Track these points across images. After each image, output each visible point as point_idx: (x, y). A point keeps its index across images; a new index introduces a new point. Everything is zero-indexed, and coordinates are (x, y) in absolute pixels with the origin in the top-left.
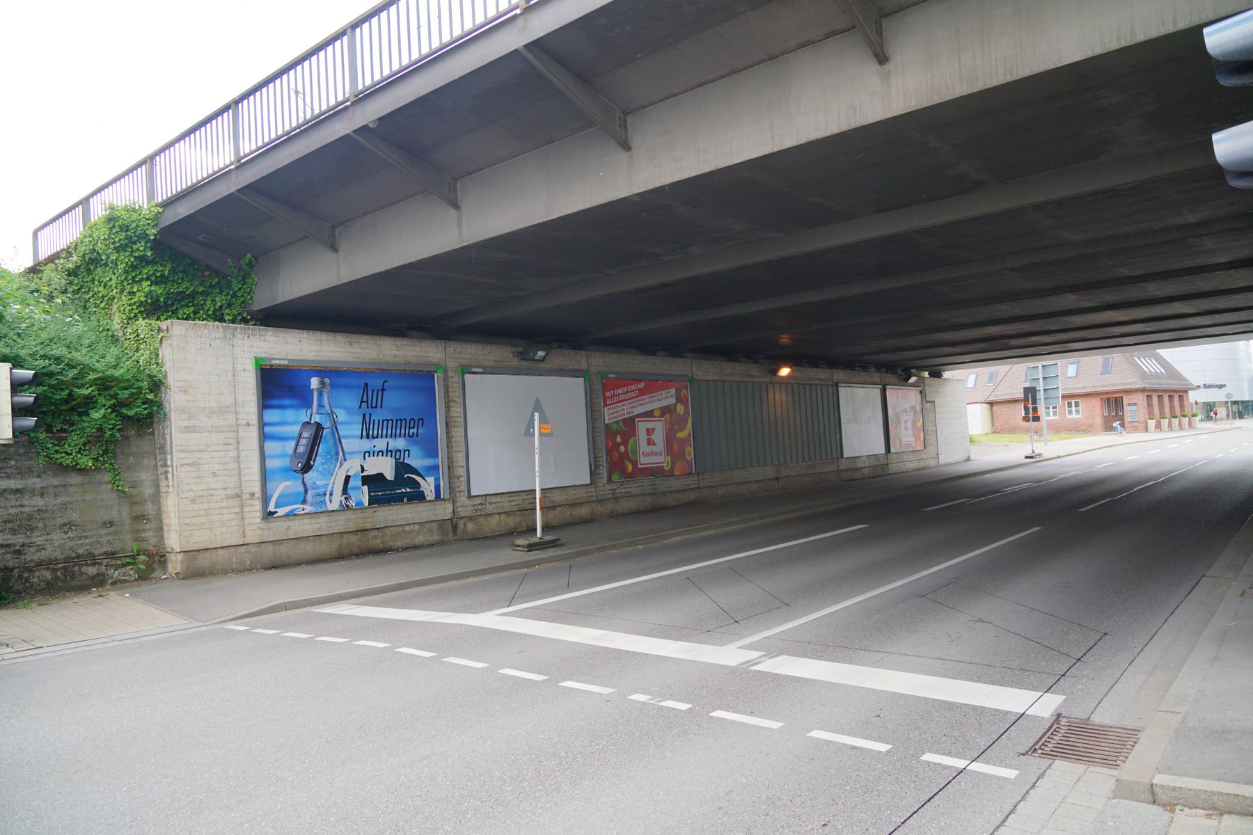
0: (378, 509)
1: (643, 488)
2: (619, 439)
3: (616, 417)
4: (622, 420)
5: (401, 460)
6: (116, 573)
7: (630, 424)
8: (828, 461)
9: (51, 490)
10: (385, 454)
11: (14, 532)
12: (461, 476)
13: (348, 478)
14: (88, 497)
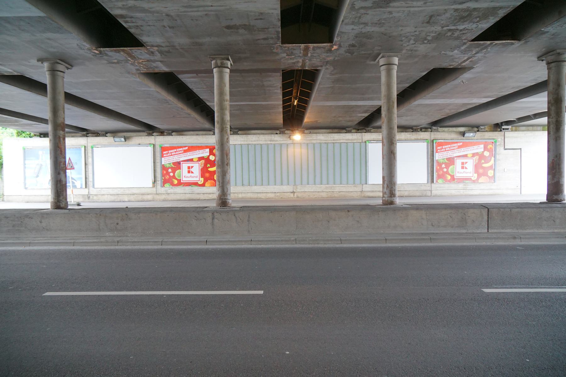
2: (170, 170)
7: (177, 165)
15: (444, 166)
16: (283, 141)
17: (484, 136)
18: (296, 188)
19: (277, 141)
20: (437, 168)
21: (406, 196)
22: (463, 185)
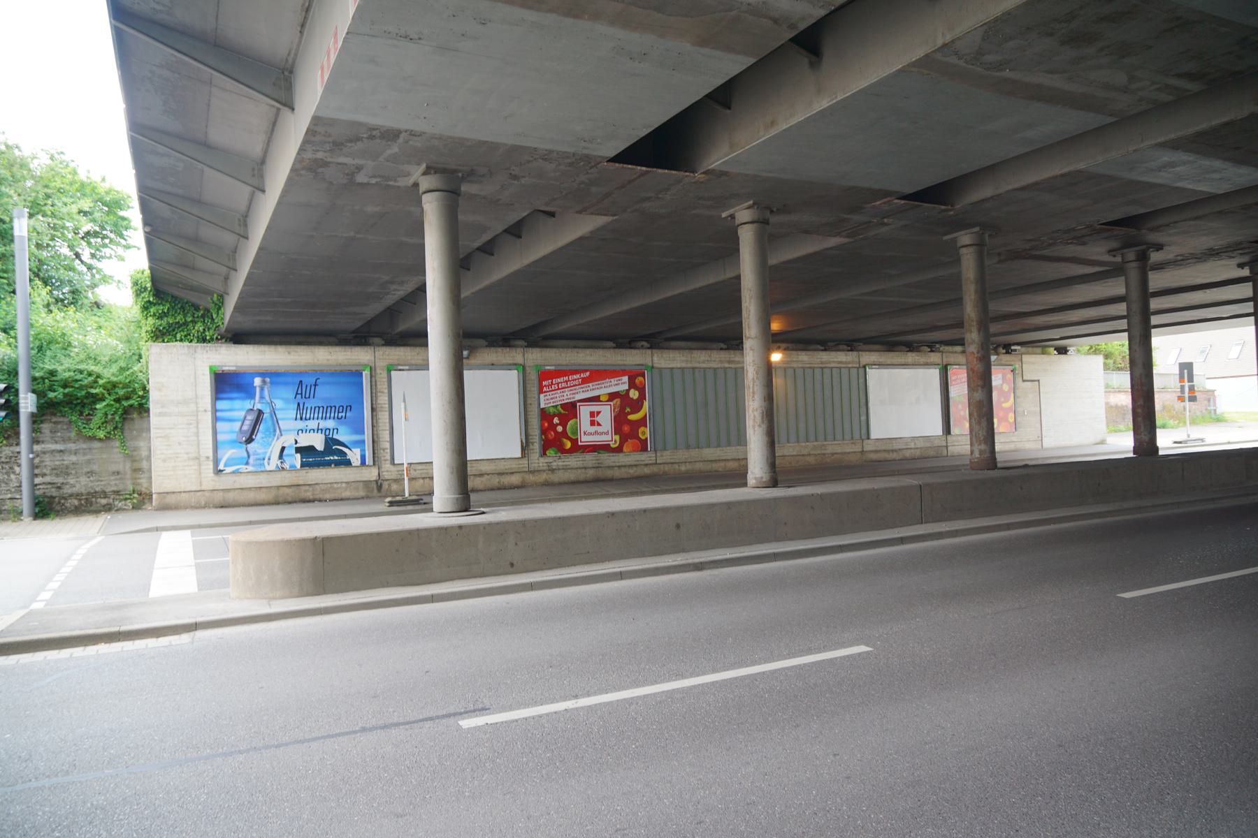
0: (309, 471)
1: (584, 462)
2: (556, 420)
3: (553, 402)
4: (561, 404)
5: (331, 436)
6: (120, 504)
7: (570, 410)
8: (846, 442)
9: (81, 451)
10: (316, 431)
11: (57, 475)
12: (387, 449)
13: (283, 448)
14: (104, 456)
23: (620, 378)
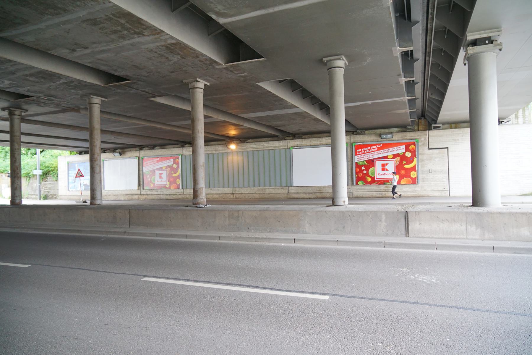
2: (363, 168)
4: (366, 160)
7: (371, 163)
15: (364, 169)
16: (224, 150)
17: (406, 136)
18: (234, 190)
19: (220, 150)
20: (356, 170)
21: (327, 198)
22: (384, 187)
23: (400, 147)
